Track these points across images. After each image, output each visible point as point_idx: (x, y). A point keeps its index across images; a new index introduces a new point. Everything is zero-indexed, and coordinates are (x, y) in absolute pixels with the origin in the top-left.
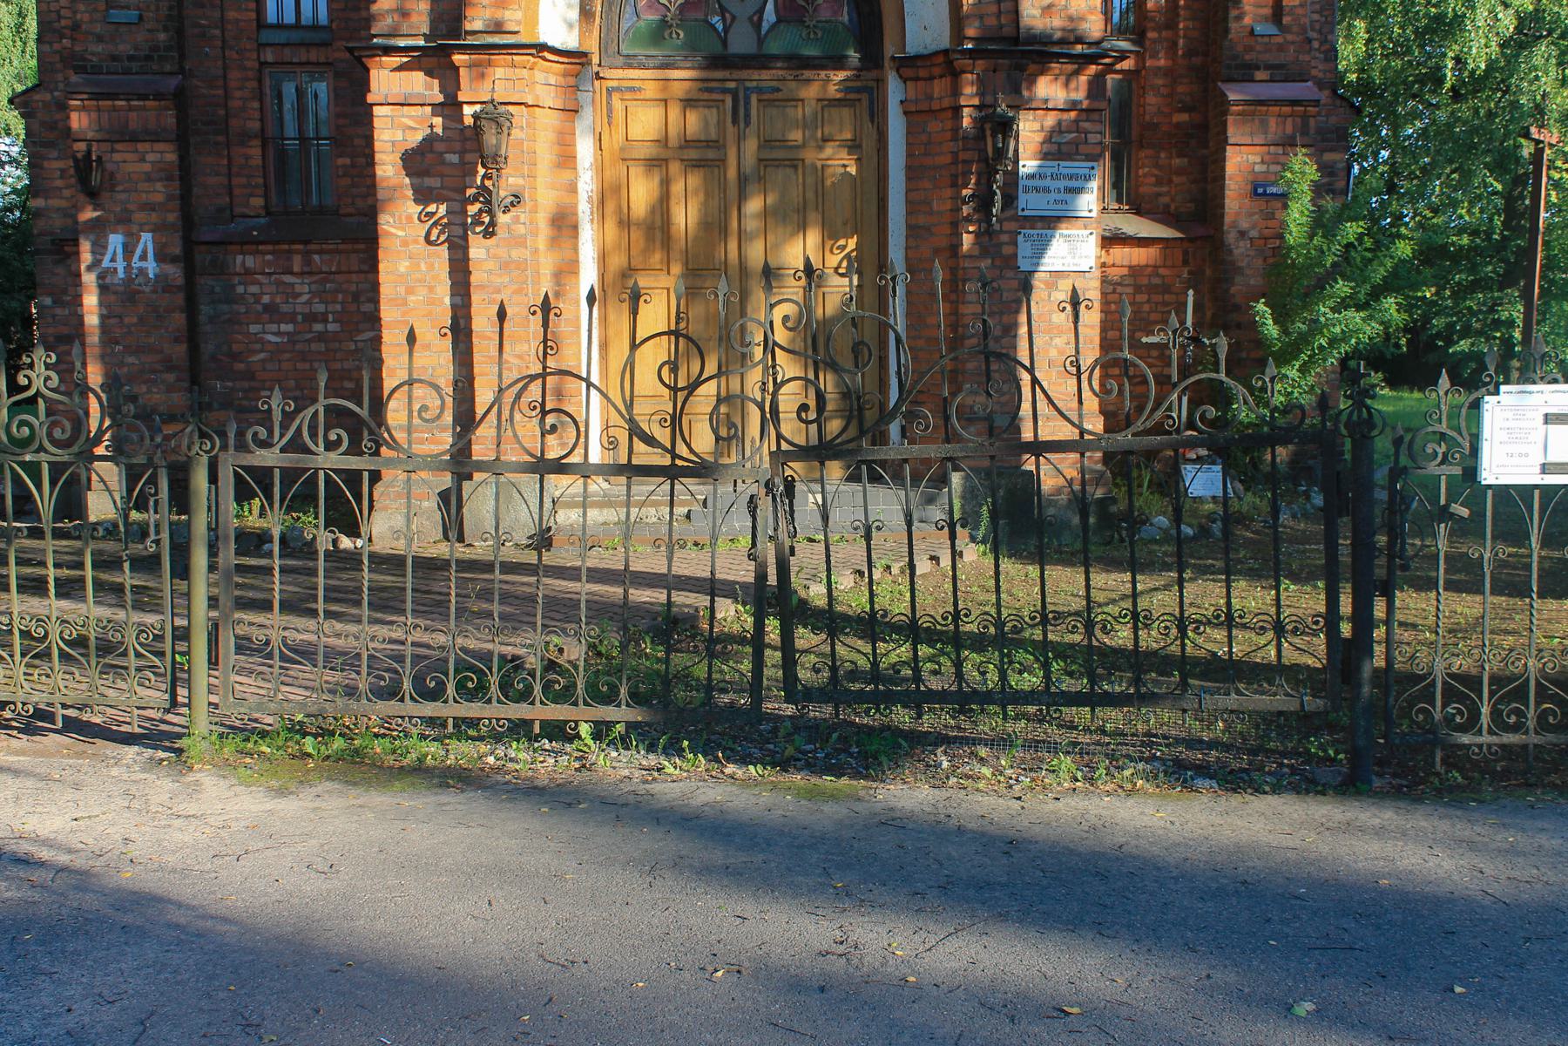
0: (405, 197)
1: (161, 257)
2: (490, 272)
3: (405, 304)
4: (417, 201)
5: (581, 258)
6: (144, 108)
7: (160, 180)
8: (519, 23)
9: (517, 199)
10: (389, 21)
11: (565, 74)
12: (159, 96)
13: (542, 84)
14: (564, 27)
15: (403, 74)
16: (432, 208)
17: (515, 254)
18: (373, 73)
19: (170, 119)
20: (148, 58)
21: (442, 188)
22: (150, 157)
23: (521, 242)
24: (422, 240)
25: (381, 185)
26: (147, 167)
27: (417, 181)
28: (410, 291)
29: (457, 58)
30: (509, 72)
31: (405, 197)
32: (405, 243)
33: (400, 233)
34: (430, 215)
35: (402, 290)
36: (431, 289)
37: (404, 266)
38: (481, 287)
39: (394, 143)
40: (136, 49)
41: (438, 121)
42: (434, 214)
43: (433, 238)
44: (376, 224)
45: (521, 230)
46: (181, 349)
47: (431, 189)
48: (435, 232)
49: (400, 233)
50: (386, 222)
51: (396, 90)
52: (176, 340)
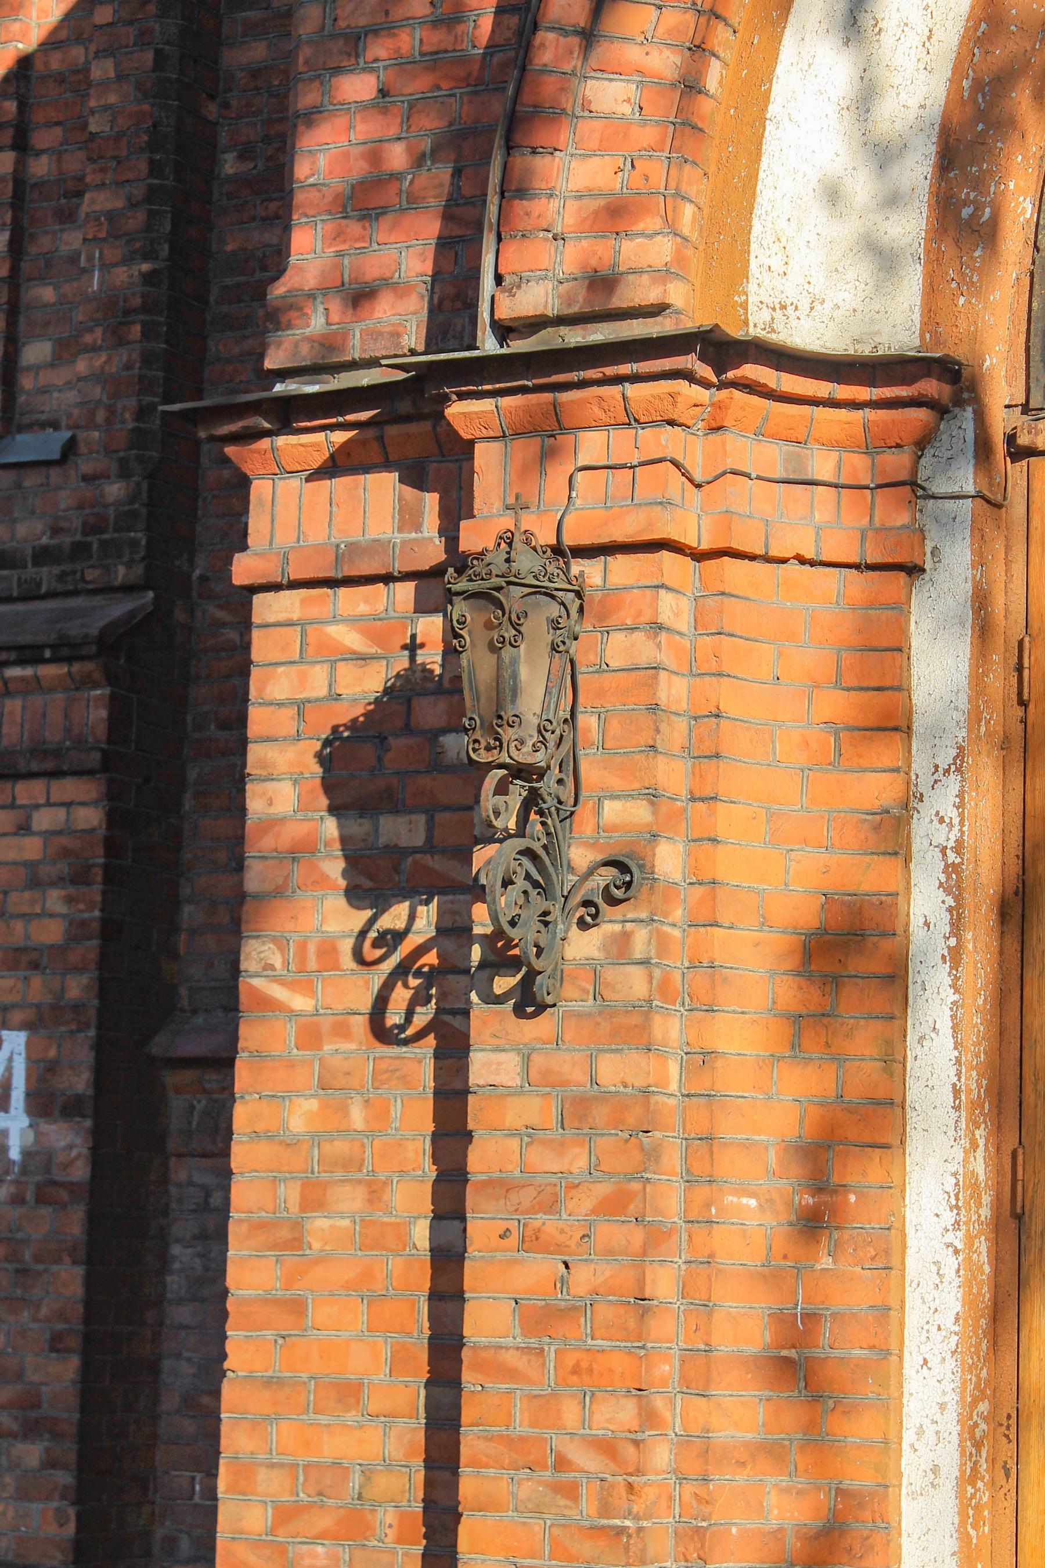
0: (323, 881)
1: (42, 1103)
2: (530, 1134)
3: (296, 1242)
4: (354, 895)
5: (914, 1092)
6: (35, 685)
7: (59, 882)
8: (664, 274)
9: (626, 873)
10: (316, 323)
11: (873, 445)
12: (65, 650)
13: (784, 483)
14: (861, 271)
15: (341, 484)
16: (395, 917)
17: (615, 1070)
18: (260, 489)
19: (94, 712)
20: (80, 550)
21: (430, 847)
22: (44, 820)
23: (630, 1027)
24: (360, 1025)
25: (259, 846)
26: (31, 848)
27: (359, 828)
28: (314, 1198)
29: (465, 413)
30: (622, 444)
31: (323, 881)
32: (310, 1036)
33: (300, 1003)
34: (392, 939)
35: (290, 1194)
36: (375, 1191)
37: (301, 1114)
38: (502, 1187)
39: (301, 706)
40: (55, 531)
41: (431, 627)
42: (400, 936)
43: (394, 1018)
44: (235, 971)
45: (635, 983)
46: (59, 1376)
47: (396, 853)
48: (401, 996)
49: (300, 1003)
50: (262, 961)
51: (317, 535)
52: (56, 1344)
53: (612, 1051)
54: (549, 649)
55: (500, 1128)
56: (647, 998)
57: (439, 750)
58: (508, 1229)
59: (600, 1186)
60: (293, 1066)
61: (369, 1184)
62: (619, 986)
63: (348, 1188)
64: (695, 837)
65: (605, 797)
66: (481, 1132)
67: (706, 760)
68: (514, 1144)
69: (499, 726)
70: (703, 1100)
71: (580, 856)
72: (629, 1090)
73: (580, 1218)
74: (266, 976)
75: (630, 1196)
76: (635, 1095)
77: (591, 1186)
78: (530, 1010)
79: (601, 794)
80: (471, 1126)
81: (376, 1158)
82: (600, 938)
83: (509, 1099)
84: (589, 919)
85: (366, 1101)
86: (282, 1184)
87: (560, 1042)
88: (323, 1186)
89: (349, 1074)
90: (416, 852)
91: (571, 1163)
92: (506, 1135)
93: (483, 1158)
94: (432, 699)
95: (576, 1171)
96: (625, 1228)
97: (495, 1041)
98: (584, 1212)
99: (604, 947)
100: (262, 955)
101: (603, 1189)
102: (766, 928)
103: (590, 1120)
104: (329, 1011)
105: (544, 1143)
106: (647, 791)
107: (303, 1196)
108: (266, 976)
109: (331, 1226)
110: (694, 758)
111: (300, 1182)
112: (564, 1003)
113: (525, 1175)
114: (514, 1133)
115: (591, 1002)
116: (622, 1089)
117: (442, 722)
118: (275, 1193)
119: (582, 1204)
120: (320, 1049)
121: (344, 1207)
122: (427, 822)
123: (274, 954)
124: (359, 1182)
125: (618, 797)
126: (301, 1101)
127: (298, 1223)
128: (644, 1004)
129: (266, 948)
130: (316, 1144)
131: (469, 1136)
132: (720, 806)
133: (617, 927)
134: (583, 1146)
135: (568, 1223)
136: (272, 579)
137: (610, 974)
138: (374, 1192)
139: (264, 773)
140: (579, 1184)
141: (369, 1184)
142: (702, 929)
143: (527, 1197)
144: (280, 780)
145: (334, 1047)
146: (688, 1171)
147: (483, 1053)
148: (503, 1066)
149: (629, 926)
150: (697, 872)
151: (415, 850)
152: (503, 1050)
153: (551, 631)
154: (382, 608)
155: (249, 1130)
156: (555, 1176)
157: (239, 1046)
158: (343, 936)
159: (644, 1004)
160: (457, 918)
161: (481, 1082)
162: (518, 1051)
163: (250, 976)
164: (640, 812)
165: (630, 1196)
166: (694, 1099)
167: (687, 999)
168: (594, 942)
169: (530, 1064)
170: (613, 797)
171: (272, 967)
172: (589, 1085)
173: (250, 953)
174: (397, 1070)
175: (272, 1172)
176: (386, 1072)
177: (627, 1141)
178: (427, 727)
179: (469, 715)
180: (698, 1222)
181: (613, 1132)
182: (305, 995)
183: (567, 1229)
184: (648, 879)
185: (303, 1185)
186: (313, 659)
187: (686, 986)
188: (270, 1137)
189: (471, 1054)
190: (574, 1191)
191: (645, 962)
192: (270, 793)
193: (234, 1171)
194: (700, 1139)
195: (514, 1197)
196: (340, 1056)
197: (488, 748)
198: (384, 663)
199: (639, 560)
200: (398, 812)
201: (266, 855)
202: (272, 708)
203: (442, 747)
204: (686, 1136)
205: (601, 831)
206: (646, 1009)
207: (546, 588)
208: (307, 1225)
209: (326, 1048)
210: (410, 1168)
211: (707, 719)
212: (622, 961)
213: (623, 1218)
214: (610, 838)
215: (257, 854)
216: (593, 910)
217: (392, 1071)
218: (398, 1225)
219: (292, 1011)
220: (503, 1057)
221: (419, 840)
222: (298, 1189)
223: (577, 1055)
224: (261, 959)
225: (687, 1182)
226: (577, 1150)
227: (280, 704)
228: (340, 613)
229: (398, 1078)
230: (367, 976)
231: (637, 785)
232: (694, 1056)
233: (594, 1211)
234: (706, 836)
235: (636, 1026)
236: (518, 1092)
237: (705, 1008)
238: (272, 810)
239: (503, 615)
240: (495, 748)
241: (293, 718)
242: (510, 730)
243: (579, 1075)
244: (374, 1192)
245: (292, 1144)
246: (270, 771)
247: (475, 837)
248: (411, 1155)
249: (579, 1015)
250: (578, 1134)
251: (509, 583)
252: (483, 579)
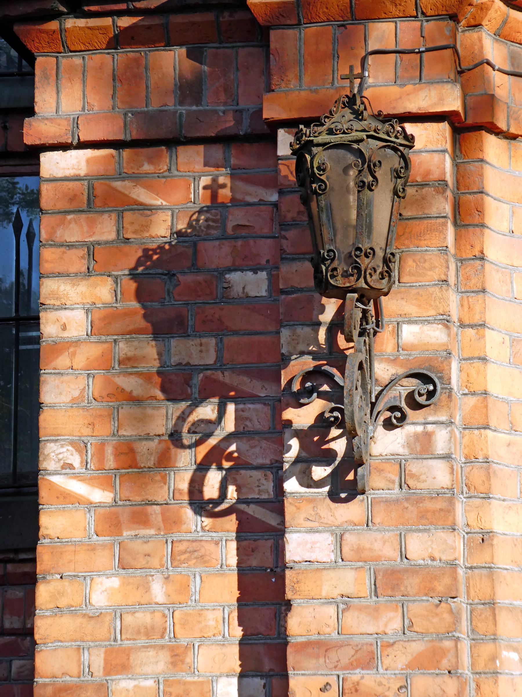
2: (345, 603)
9: (426, 386)
23: (434, 511)
28: (119, 663)
35: (97, 660)
36: (178, 655)
38: (319, 647)
53: (419, 531)
54: (391, 194)
55: (317, 597)
56: (450, 487)
57: (226, 285)
58: (327, 683)
59: (414, 644)
60: (94, 550)
61: (172, 649)
62: (423, 477)
63: (152, 653)
64: (465, 356)
65: (404, 322)
66: (299, 601)
67: (473, 294)
68: (332, 610)
69: (357, 256)
70: (484, 572)
71: (383, 371)
72: (436, 563)
73: (397, 672)
74: (65, 474)
75: (443, 653)
76: (443, 567)
77: (406, 644)
78: (343, 495)
79: (400, 319)
80: (289, 595)
81: (177, 627)
82: (404, 437)
83: (325, 572)
84: (394, 421)
85: (167, 578)
86: (86, 652)
87: (370, 524)
88: (127, 652)
89: (149, 555)
90: (207, 369)
91: (386, 625)
92: (324, 603)
93: (302, 623)
94: (217, 243)
95: (389, 631)
96: (439, 680)
97: (309, 524)
98: (400, 666)
99: (408, 445)
100: (61, 456)
101: (417, 647)
102: (513, 432)
103: (402, 589)
104: (128, 503)
105: (360, 609)
106: (441, 317)
107: (106, 661)
108: (65, 474)
109: (135, 686)
110: (462, 292)
111: (103, 650)
112: (372, 491)
113: (342, 637)
114: (330, 601)
115: (397, 490)
116: (430, 562)
117: (228, 262)
118: (80, 659)
119: (398, 660)
120: (121, 535)
121: (148, 669)
122: (217, 344)
123: (72, 455)
124: (163, 647)
125: (415, 322)
126: (103, 579)
127: (103, 685)
128: (447, 491)
129: (64, 450)
130: (118, 615)
131: (288, 605)
132: (488, 332)
133: (419, 429)
134: (396, 610)
135: (386, 676)
136: (62, 140)
137: (414, 467)
138: (176, 655)
139: (58, 303)
140: (395, 643)
141: (172, 649)
142: (476, 432)
143: (345, 655)
144: (73, 309)
145: (133, 533)
146: (473, 630)
147: (298, 535)
148: (318, 545)
149: (430, 427)
150: (469, 385)
151: (207, 368)
152: (317, 532)
153: (394, 179)
154: (166, 168)
155: (52, 606)
156: (371, 637)
157: (40, 533)
158: (140, 439)
159: (447, 491)
160: (248, 423)
161: (297, 559)
162: (332, 533)
163: (50, 474)
164: (436, 335)
165: (443, 653)
166: (476, 571)
167: (465, 489)
168: (398, 441)
169: (343, 543)
170: (410, 322)
171: (71, 466)
172: (399, 559)
173: (48, 455)
174: (195, 551)
175: (75, 641)
176: (185, 552)
177: (437, 606)
178: (213, 267)
179: (327, 247)
180: (485, 673)
181: (424, 598)
182: (104, 490)
183: (385, 682)
184: (446, 388)
185: (106, 652)
186: (101, 209)
187: (464, 478)
188: (72, 611)
189: (287, 535)
190: (389, 650)
191: (447, 457)
192: (64, 320)
193: (38, 642)
194: (483, 604)
195: (333, 656)
196: (139, 541)
197: (346, 275)
198: (170, 213)
199: (426, 129)
200: (189, 336)
201: (62, 371)
202: (63, 249)
203: (229, 282)
204: (470, 601)
205: (400, 349)
206: (448, 496)
207: (394, 142)
208: (113, 686)
209: (125, 534)
210: (211, 634)
211: (472, 262)
212: (425, 456)
213: (437, 671)
214: (410, 355)
215: (53, 371)
216: (398, 414)
217: (190, 552)
218: (202, 683)
219: (91, 503)
220: (317, 537)
221: (210, 360)
222: (102, 655)
223: (387, 535)
224: (60, 460)
225: (473, 640)
226: (392, 614)
227: (70, 246)
228: (125, 171)
229: (196, 558)
230: (164, 473)
231: (432, 312)
232: (474, 535)
233: (409, 666)
234: (476, 355)
235: (441, 510)
236: (333, 566)
237: (482, 495)
238: (65, 334)
239: (363, 164)
240: (352, 275)
241: (83, 258)
242: (367, 261)
243: (390, 551)
244: (176, 655)
245: (97, 617)
246: (63, 301)
247: (283, 354)
248: (212, 623)
249: (388, 502)
250: (392, 601)
251: (368, 137)
252: (344, 133)
